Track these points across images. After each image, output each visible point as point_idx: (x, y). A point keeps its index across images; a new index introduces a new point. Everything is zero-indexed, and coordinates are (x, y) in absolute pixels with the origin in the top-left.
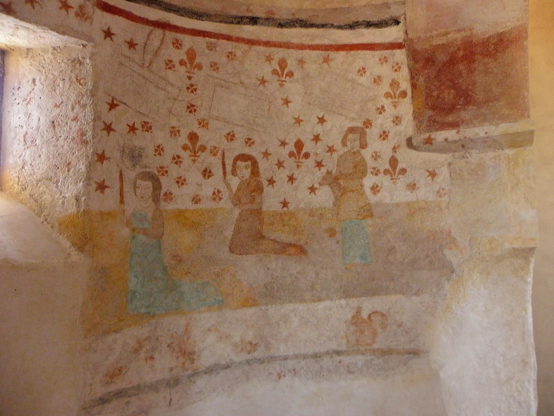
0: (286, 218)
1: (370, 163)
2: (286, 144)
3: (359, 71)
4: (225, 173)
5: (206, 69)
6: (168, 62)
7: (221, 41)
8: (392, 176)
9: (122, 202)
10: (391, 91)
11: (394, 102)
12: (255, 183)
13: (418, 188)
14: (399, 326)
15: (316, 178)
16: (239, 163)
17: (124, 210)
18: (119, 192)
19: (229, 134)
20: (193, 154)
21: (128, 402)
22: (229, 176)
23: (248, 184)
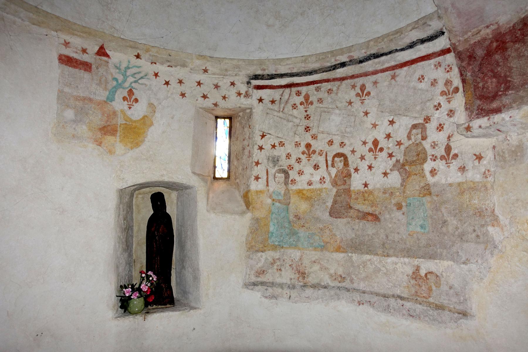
0: (366, 195)
1: (430, 151)
2: (367, 143)
3: (419, 79)
4: (327, 166)
5: (315, 104)
6: (293, 105)
8: (446, 161)
9: (267, 185)
10: (446, 90)
12: (346, 172)
13: (467, 170)
14: (451, 288)
15: (389, 166)
16: (336, 159)
19: (330, 141)
20: (308, 156)
22: (330, 168)
23: (342, 172)
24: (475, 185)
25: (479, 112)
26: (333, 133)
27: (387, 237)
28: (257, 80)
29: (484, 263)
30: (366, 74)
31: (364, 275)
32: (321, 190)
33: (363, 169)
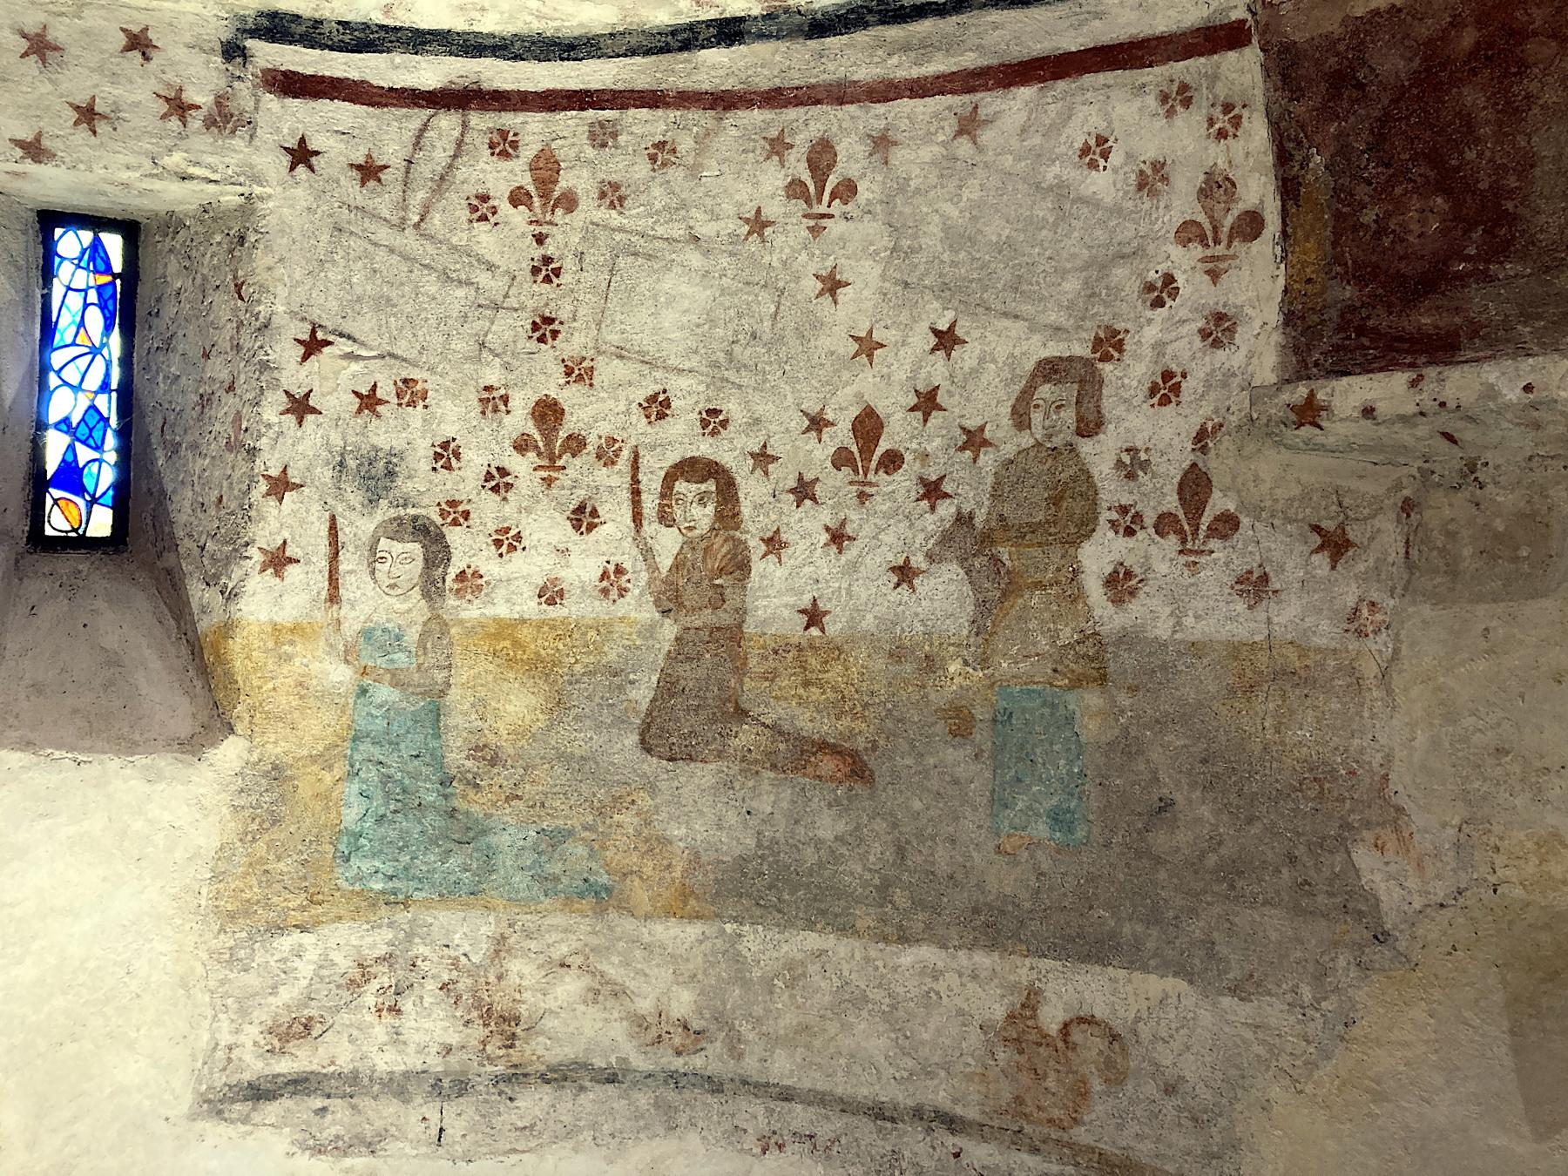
0: (814, 662)
1: (1112, 490)
3: (1085, 151)
4: (637, 518)
5: (590, 210)
6: (475, 202)
7: (632, 112)
9: (334, 598)
10: (1201, 218)
11: (1213, 258)
12: (724, 550)
13: (1275, 592)
14: (1170, 1090)
15: (921, 536)
16: (681, 486)
17: (338, 621)
18: (327, 575)
19: (653, 399)
20: (545, 462)
21: (323, 1110)
22: (651, 528)
24: (1308, 662)
25: (1349, 338)
26: (672, 362)
27: (901, 852)
28: (281, 41)
29: (1325, 999)
30: (840, 94)
31: (789, 1019)
32: (603, 628)
33: (803, 545)
